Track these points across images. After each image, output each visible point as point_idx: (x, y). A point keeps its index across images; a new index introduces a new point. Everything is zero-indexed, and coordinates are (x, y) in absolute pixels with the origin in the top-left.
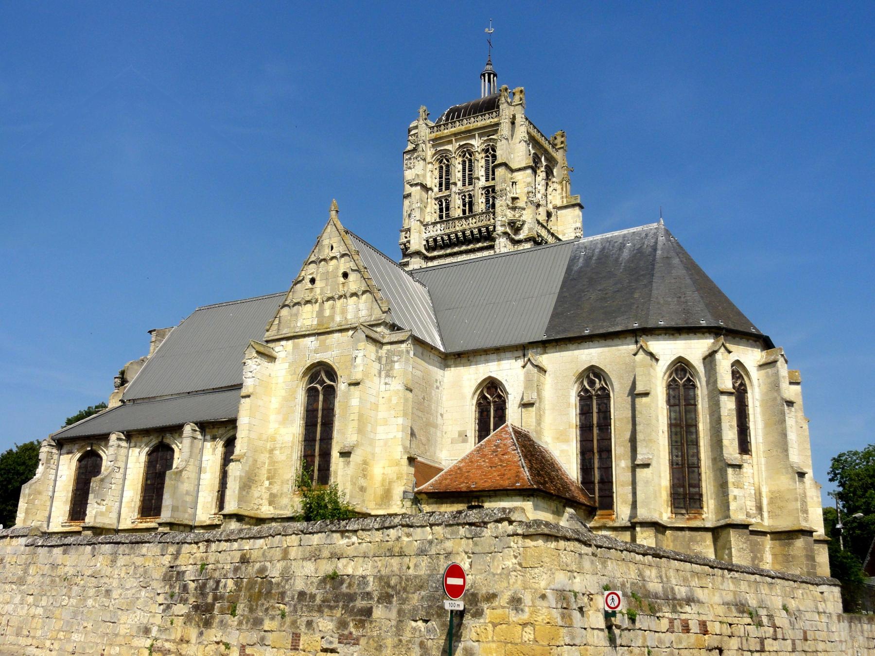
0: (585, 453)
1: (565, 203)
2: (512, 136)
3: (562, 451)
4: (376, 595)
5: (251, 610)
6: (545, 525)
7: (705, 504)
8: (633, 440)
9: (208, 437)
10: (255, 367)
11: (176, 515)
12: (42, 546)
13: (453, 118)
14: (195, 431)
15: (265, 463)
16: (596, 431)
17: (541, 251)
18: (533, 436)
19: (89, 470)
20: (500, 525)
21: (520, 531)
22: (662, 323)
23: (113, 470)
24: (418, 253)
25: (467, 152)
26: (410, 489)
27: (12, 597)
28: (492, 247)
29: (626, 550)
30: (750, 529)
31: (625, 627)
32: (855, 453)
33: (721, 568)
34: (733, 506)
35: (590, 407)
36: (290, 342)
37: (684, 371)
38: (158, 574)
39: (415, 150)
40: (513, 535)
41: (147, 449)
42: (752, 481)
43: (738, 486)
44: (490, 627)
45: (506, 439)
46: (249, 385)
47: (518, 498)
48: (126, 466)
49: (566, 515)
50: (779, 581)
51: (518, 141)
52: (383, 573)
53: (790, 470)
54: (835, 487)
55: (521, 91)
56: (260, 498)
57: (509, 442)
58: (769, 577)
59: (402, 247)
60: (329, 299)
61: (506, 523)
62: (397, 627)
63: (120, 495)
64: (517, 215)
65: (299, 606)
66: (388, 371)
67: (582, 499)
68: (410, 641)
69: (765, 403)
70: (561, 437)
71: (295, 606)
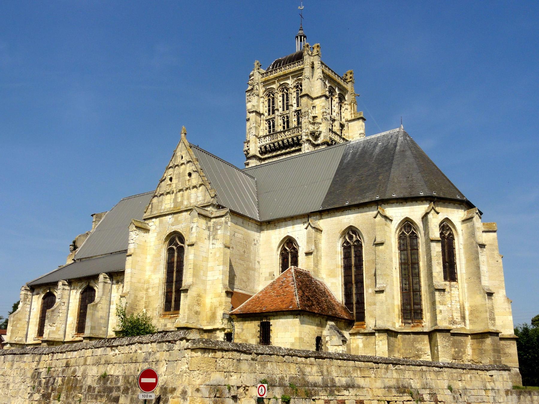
0: (347, 284)
1: (353, 118)
2: (312, 76)
3: (332, 283)
4: (122, 388)
5: (67, 398)
7: (424, 316)
10: (135, 236)
11: (94, 332)
13: (276, 67)
14: (106, 278)
16: (353, 269)
17: (332, 150)
18: (312, 274)
19: (49, 302)
20: (182, 342)
22: (394, 196)
23: (60, 304)
24: (254, 157)
28: (300, 150)
29: (288, 355)
30: (451, 332)
33: (385, 363)
34: (439, 317)
35: (350, 253)
36: (158, 219)
37: (410, 226)
38: (29, 375)
39: (252, 89)
41: (80, 290)
42: (458, 299)
43: (442, 304)
45: (289, 277)
46: (131, 248)
47: (290, 316)
48: (70, 299)
49: (328, 326)
50: (446, 369)
51: (316, 79)
55: (318, 46)
57: (291, 279)
58: (437, 367)
59: (245, 153)
60: (180, 190)
61: (184, 341)
64: (316, 128)
66: (214, 236)
70: (332, 274)
71: (86, 395)
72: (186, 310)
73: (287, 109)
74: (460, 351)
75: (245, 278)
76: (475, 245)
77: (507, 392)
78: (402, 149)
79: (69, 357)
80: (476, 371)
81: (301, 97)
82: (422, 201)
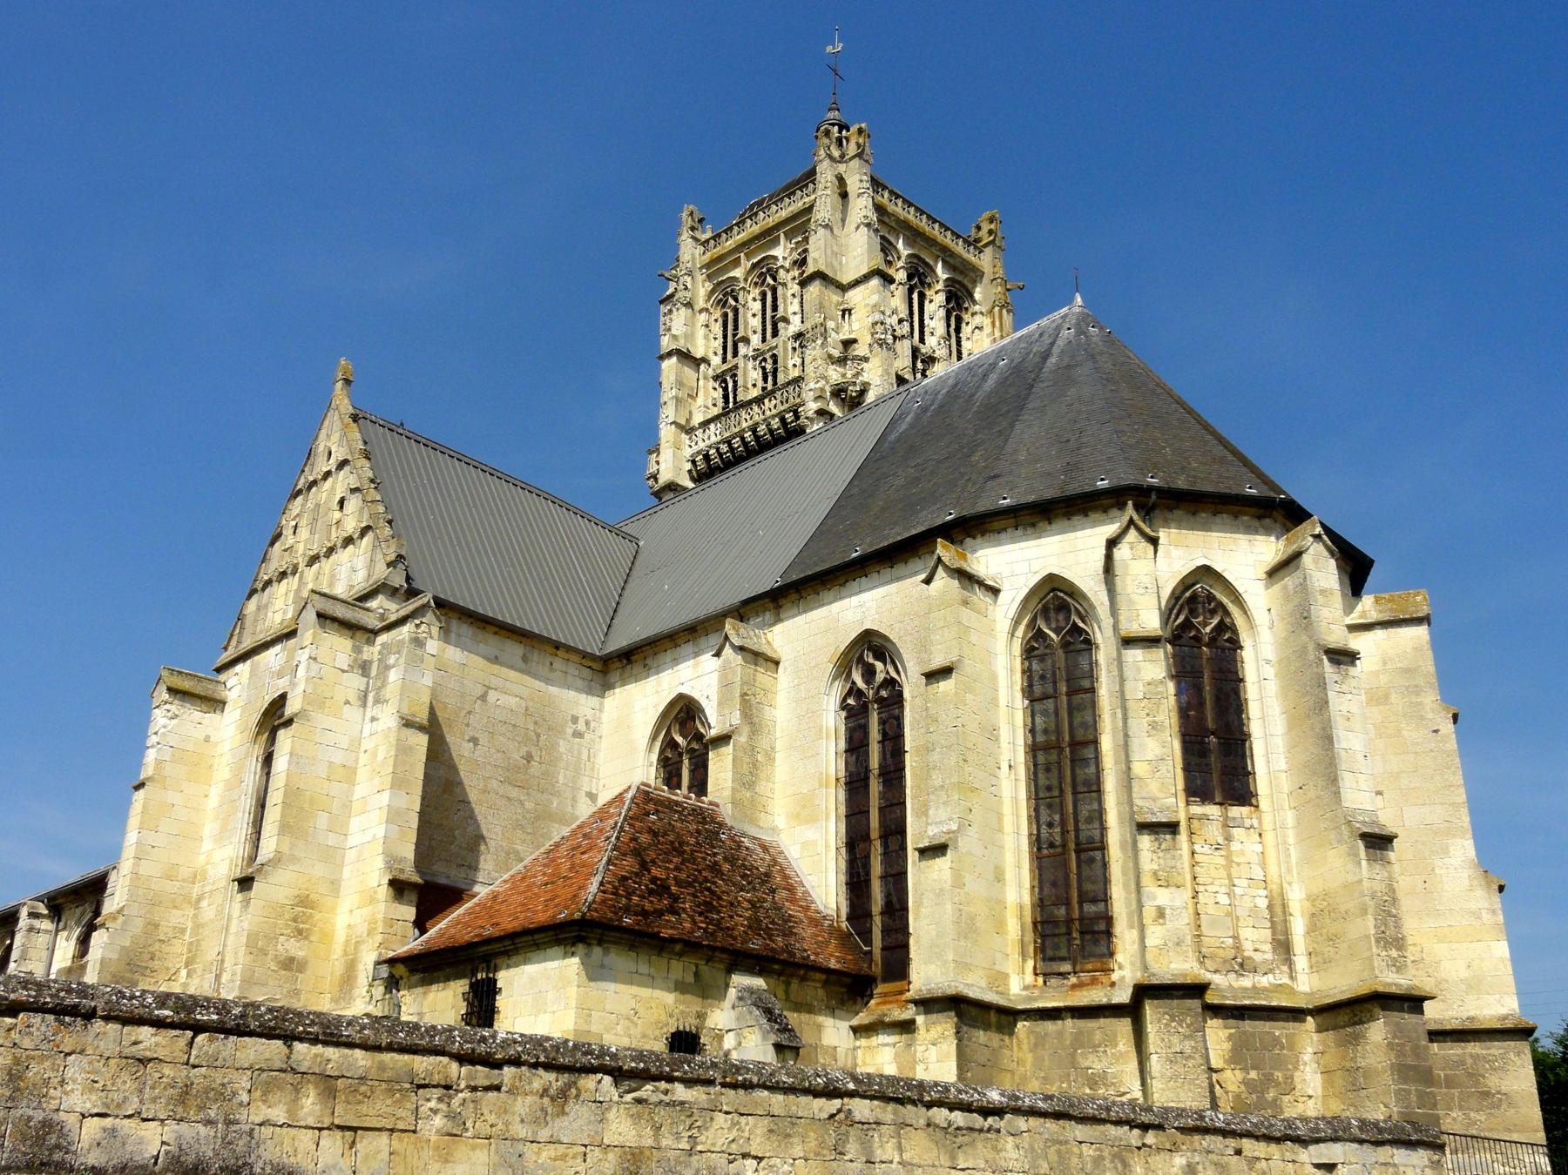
0: (856, 843)
2: (843, 221)
10: (164, 721)
15: (183, 931)
30: (1211, 998)
35: (864, 729)
37: (1063, 608)
49: (732, 993)
50: (1022, 1123)
70: (804, 813)
73: (775, 334)
74: (1268, 1080)
76: (1312, 654)
78: (1066, 360)
80: (1232, 1143)
82: (1105, 511)
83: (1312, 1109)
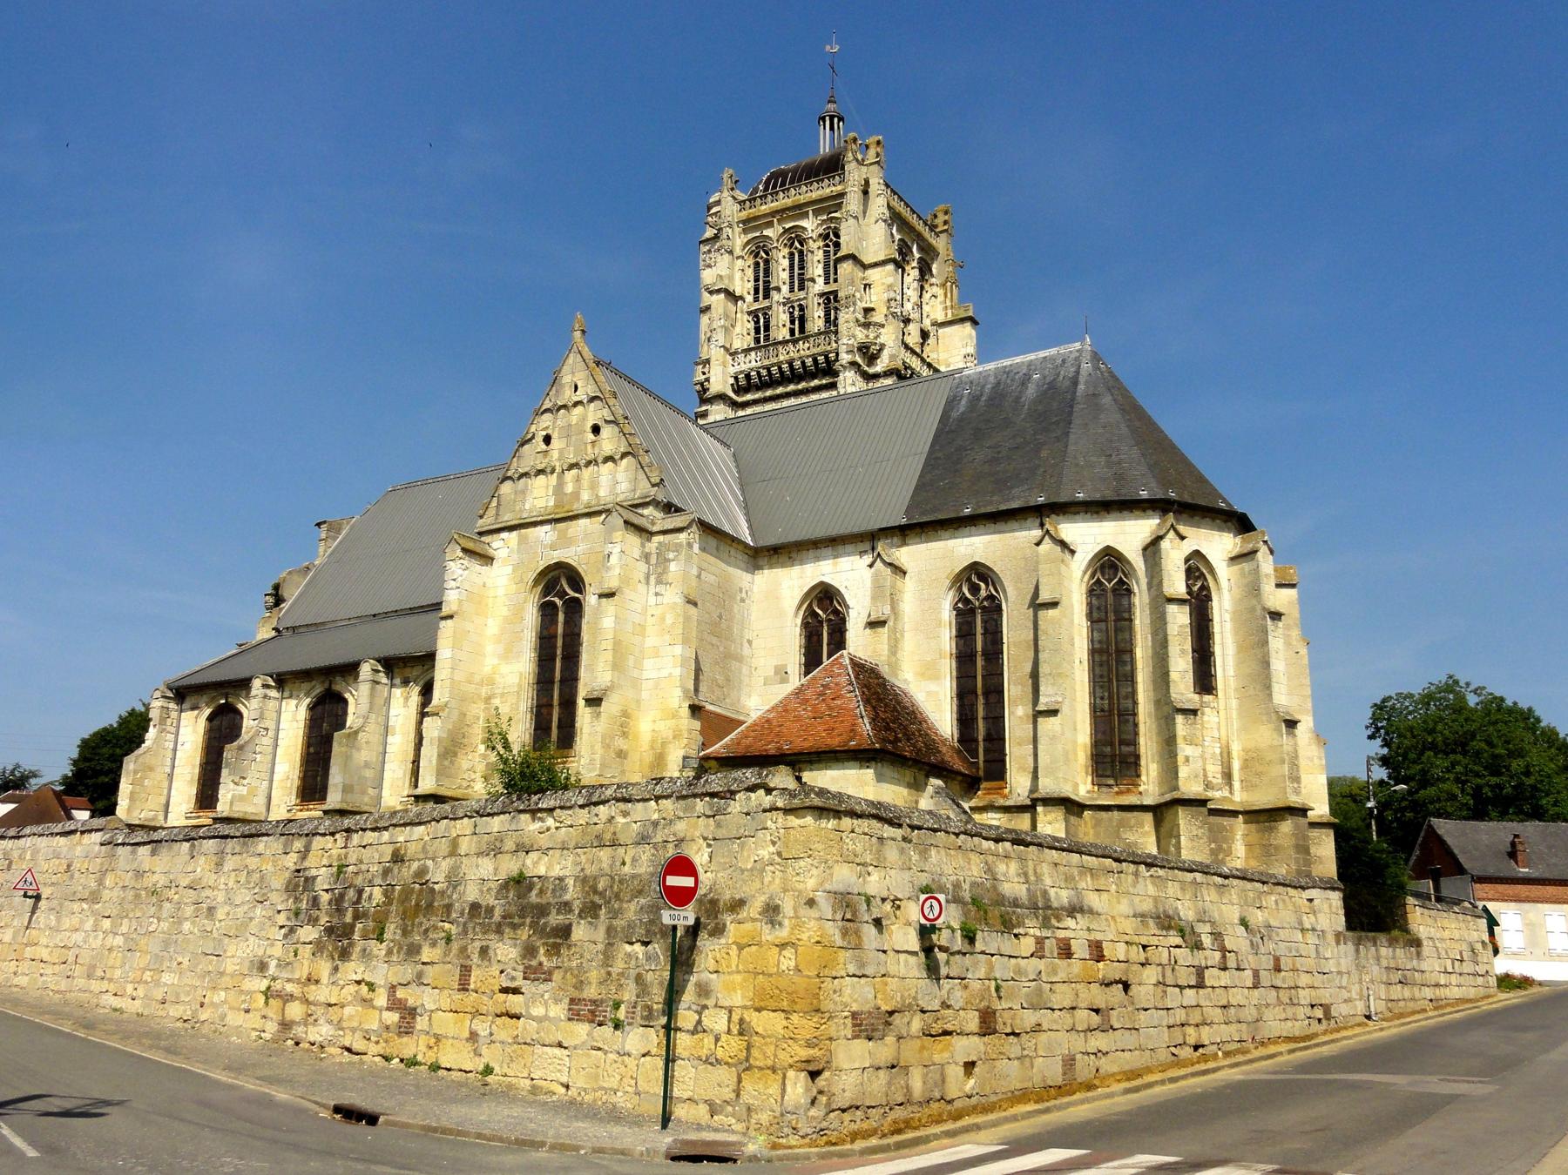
1: (950, 317)
3: (929, 693)
5: (405, 933)
6: (817, 794)
8: (1035, 676)
9: (397, 681)
11: (349, 797)
12: (123, 844)
16: (980, 662)
17: (909, 391)
18: (885, 671)
19: (224, 730)
20: (753, 795)
21: (780, 804)
23: (257, 734)
24: (721, 397)
25: (795, 238)
26: (693, 753)
27: (82, 922)
28: (833, 386)
30: (1211, 805)
31: (956, 948)
32: (1411, 696)
33: (1133, 862)
34: (1183, 772)
35: (972, 624)
36: (515, 533)
37: (1114, 567)
38: (278, 882)
39: (716, 237)
40: (770, 810)
41: (308, 700)
43: (1191, 742)
44: (734, 951)
46: (451, 601)
48: (279, 724)
49: (930, 789)
50: (1235, 882)
52: (588, 872)
53: (1274, 717)
54: (1376, 748)
55: (878, 143)
56: (472, 769)
57: (844, 679)
58: (1220, 875)
59: (698, 387)
60: (572, 466)
61: (761, 792)
62: (605, 953)
63: (268, 775)
65: (471, 925)
67: (959, 766)
68: (622, 974)
69: (1237, 616)
70: (927, 672)
72: (598, 747)
74: (1220, 849)
75: (720, 679)
76: (1259, 612)
77: (1338, 935)
79: (401, 839)
81: (838, 261)
83: (1239, 864)
